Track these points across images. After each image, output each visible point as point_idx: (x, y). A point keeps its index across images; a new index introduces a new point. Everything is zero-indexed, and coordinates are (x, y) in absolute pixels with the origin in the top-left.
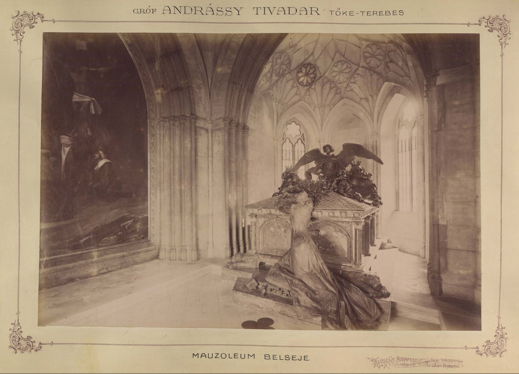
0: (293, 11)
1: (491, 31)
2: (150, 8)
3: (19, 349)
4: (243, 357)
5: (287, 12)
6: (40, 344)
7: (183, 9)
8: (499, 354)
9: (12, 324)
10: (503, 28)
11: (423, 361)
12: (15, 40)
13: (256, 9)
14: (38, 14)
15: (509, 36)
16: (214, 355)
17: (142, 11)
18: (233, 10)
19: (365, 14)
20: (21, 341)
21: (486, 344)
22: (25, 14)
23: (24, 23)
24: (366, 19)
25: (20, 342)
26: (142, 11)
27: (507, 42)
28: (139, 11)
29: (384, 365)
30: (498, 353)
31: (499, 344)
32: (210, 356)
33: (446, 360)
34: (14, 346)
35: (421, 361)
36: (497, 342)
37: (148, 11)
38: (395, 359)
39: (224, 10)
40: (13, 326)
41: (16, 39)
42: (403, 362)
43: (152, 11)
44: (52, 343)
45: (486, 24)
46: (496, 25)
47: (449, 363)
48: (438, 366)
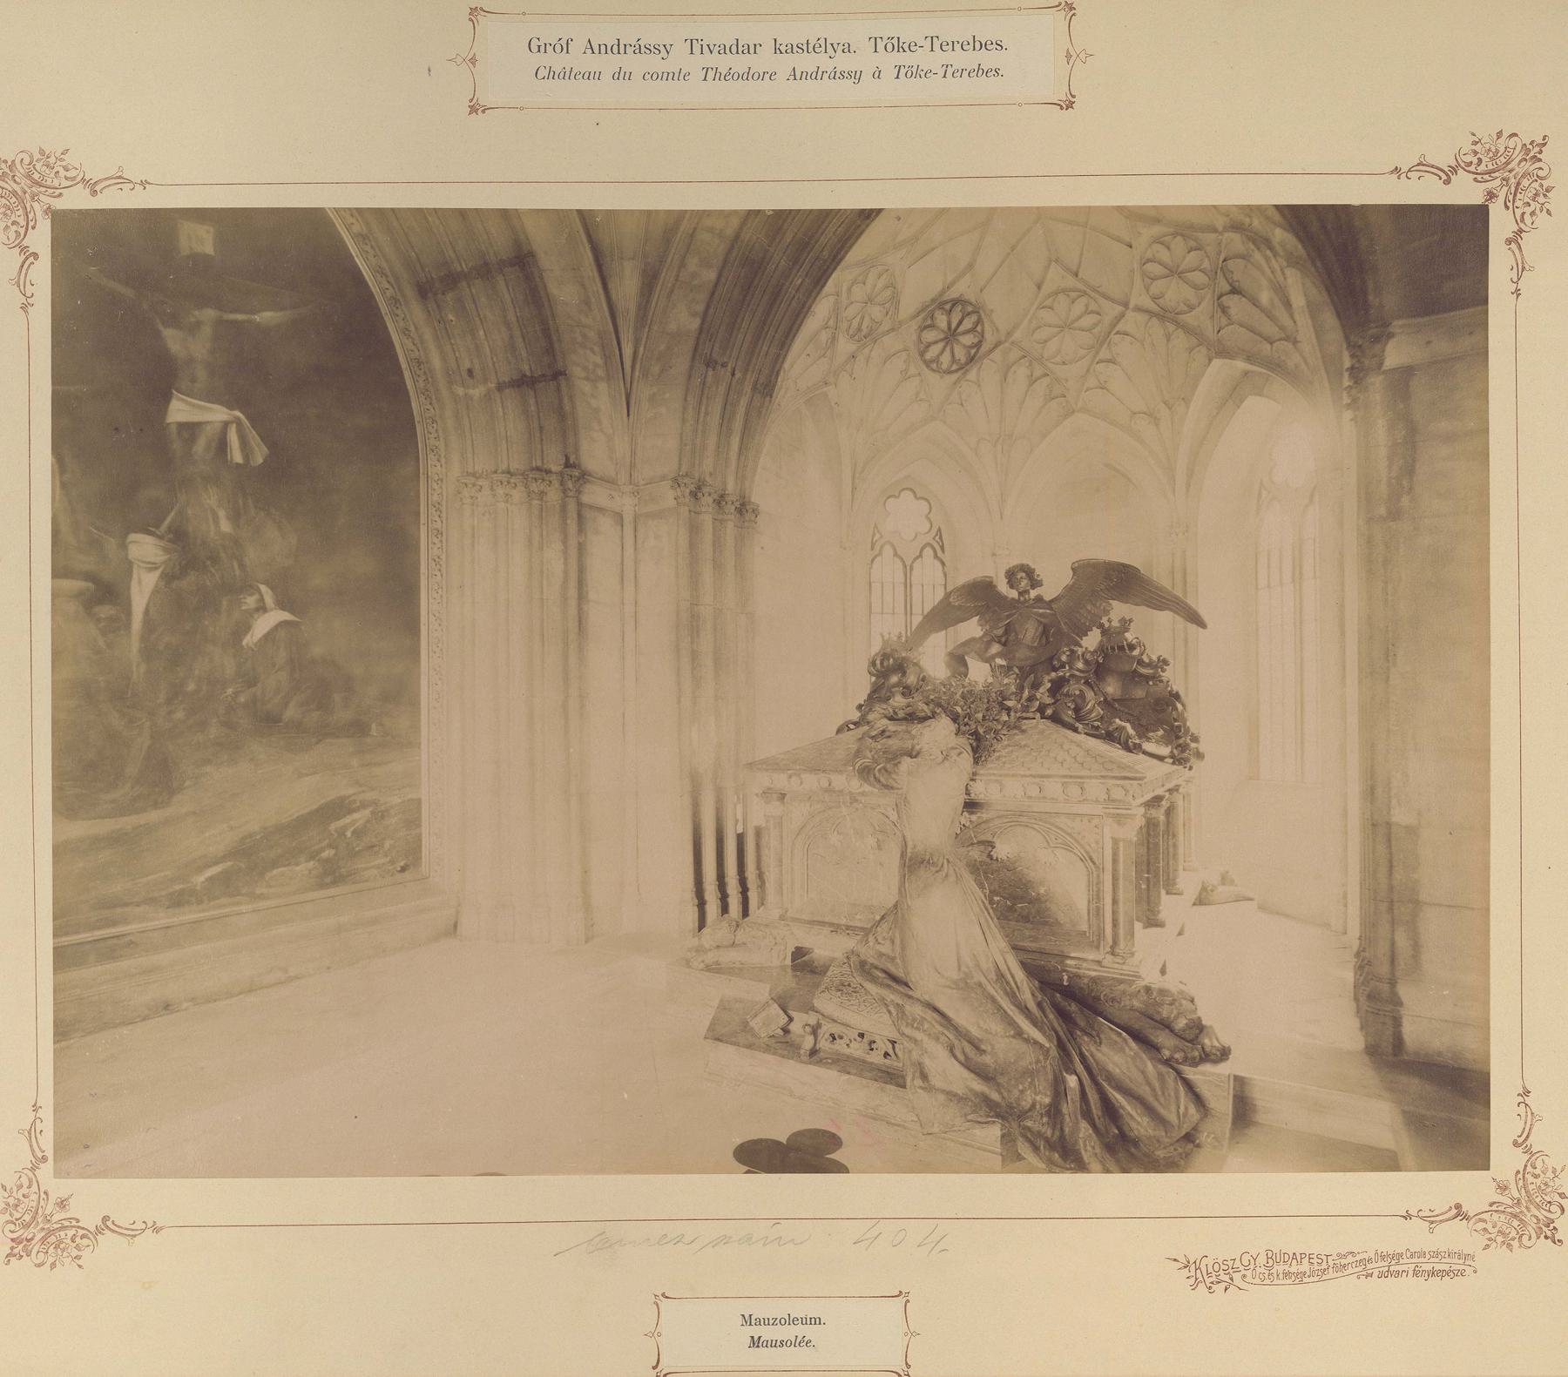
29: (1226, 1278)
35: (1343, 1261)
38: (1262, 1260)
48: (1398, 1274)
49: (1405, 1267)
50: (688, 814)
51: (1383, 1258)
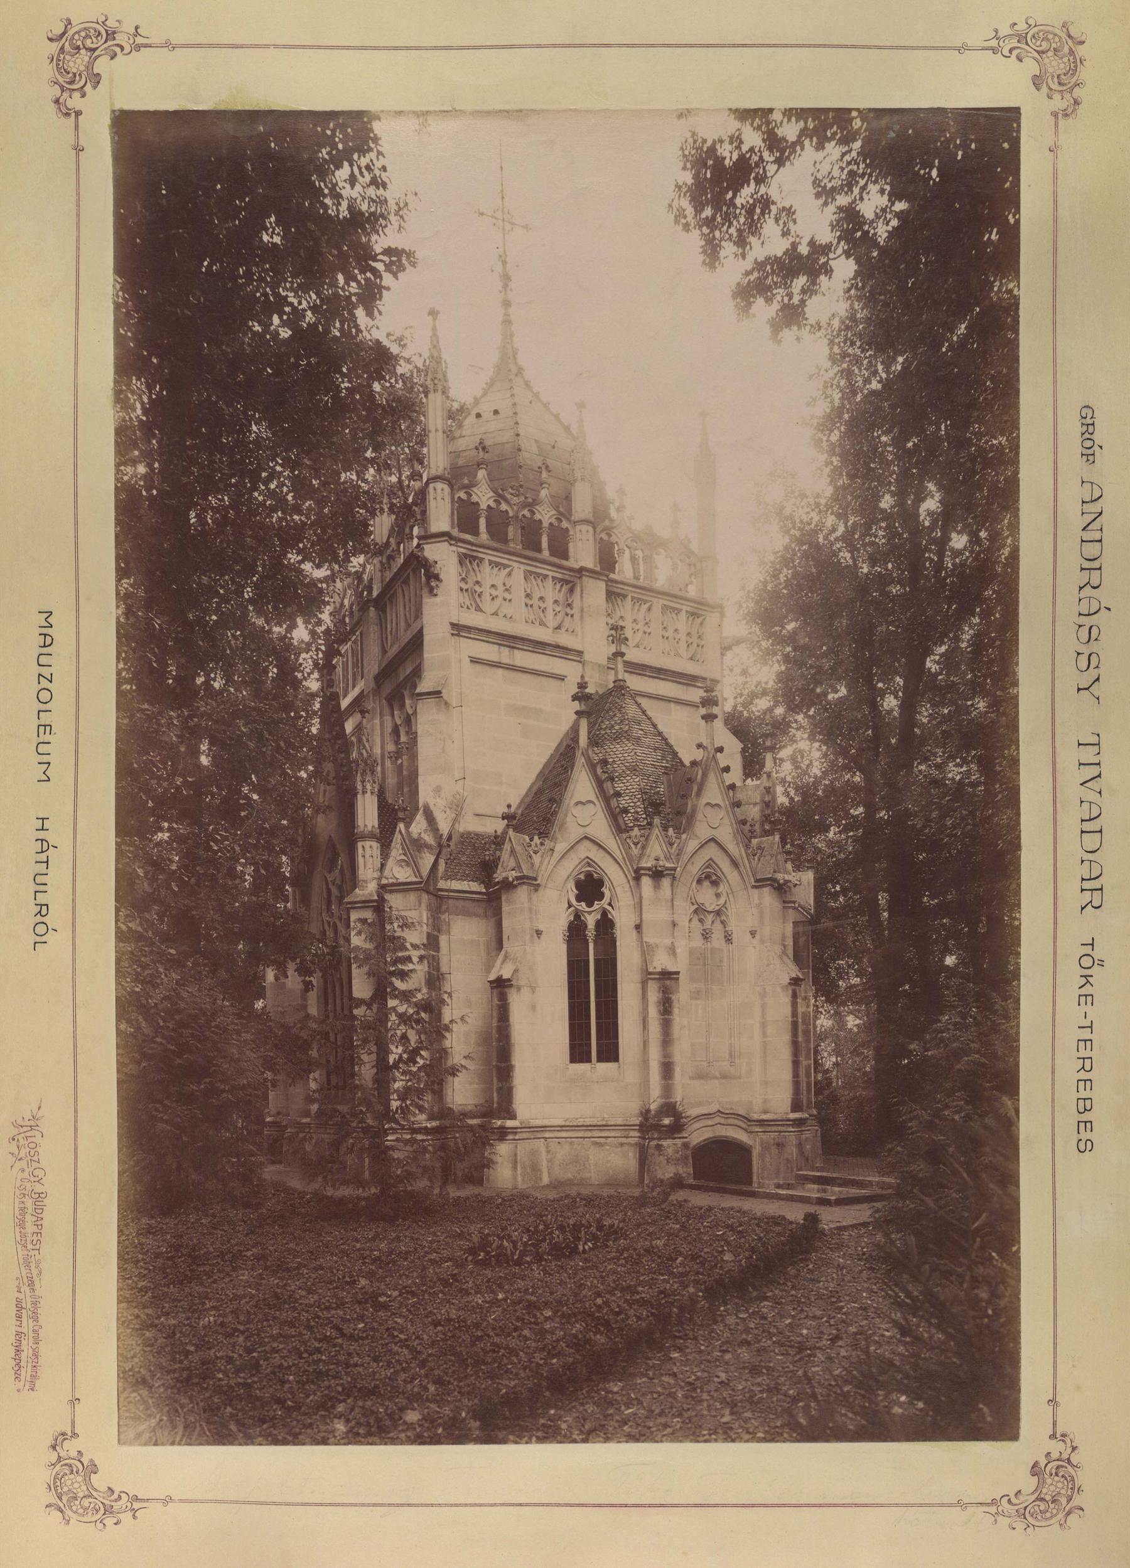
0: (1091, 841)
1: (1035, 1470)
2: (1096, 448)
3: (62, 48)
5: (1087, 826)
6: (78, 113)
7: (1097, 536)
8: (53, 1499)
9: (137, 28)
10: (1043, 1506)
11: (35, 1272)
12: (996, 31)
13: (1095, 740)
14: (1076, 103)
15: (1020, 1525)
16: (46, 671)
17: (1088, 427)
18: (1093, 673)
19: (1086, 1033)
20: (84, 55)
24: (1069, 1036)
25: (83, 51)
26: (1088, 427)
27: (1000, 1518)
28: (1088, 421)
29: (22, 1154)
30: (60, 1498)
31: (86, 1502)
32: (43, 660)
33: (37, 1341)
34: (70, 33)
35: (33, 1265)
37: (1088, 444)
38: (38, 1188)
39: (1094, 647)
41: (1001, 34)
42: (30, 1211)
43: (1090, 452)
44: (78, 149)
46: (1053, 1486)
47: (26, 1365)
48: (19, 1317)
49: (24, 1324)
50: (488, 668)
51: (35, 1303)
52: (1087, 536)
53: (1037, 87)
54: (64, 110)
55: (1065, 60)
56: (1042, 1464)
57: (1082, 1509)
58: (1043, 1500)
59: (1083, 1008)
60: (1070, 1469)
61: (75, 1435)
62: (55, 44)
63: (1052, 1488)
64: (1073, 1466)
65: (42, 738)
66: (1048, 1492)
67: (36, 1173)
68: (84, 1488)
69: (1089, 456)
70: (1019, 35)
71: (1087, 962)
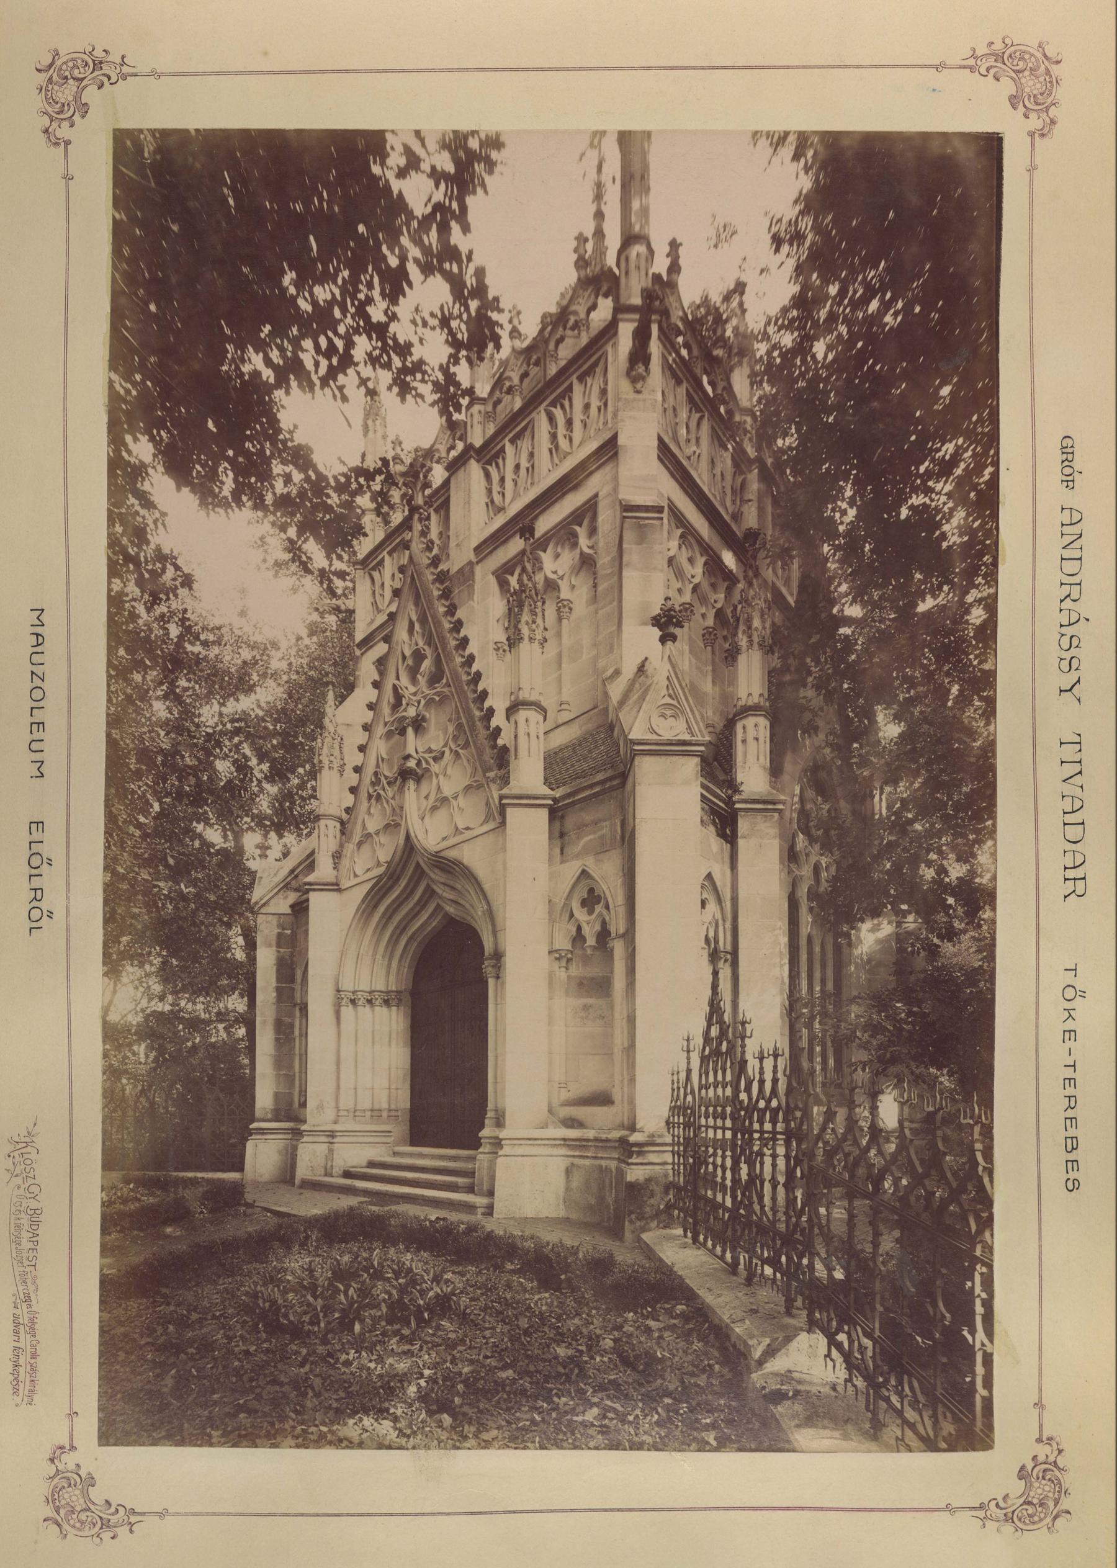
0: (1073, 832)
3: (51, 78)
4: (34, 746)
5: (1069, 818)
6: (67, 143)
9: (123, 57)
11: (31, 1288)
14: (1053, 122)
16: (38, 670)
17: (1067, 453)
18: (1073, 677)
19: (1069, 1073)
21: (83, 1473)
22: (1053, 81)
23: (1027, 81)
24: (1051, 520)
25: (71, 81)
26: (1067, 453)
27: (988, 1523)
29: (18, 1171)
31: (83, 1516)
33: (34, 1356)
34: (58, 63)
35: (29, 1281)
36: (89, 1509)
37: (1068, 471)
38: (34, 1204)
39: (1073, 652)
40: (119, 61)
44: (68, 178)
45: (1042, 1458)
46: (1040, 1489)
48: (17, 1333)
49: (22, 1339)
52: (1067, 554)
53: (1014, 107)
54: (53, 140)
55: (1042, 79)
56: (1029, 1468)
57: (1068, 1512)
58: (1029, 1503)
59: (1068, 1044)
60: (1057, 1473)
61: (73, 1448)
62: (43, 75)
63: (1039, 1491)
64: (1059, 1469)
65: (36, 736)
66: (1035, 1496)
67: (33, 1189)
68: (82, 1501)
69: (1069, 482)
70: (997, 55)
71: (1069, 993)
